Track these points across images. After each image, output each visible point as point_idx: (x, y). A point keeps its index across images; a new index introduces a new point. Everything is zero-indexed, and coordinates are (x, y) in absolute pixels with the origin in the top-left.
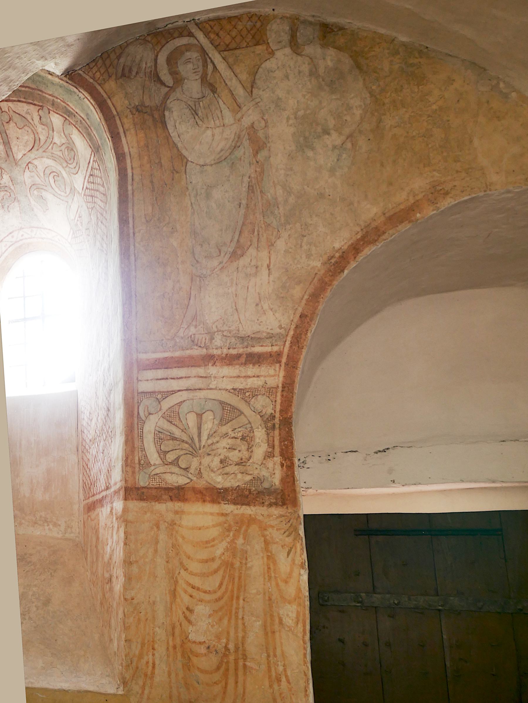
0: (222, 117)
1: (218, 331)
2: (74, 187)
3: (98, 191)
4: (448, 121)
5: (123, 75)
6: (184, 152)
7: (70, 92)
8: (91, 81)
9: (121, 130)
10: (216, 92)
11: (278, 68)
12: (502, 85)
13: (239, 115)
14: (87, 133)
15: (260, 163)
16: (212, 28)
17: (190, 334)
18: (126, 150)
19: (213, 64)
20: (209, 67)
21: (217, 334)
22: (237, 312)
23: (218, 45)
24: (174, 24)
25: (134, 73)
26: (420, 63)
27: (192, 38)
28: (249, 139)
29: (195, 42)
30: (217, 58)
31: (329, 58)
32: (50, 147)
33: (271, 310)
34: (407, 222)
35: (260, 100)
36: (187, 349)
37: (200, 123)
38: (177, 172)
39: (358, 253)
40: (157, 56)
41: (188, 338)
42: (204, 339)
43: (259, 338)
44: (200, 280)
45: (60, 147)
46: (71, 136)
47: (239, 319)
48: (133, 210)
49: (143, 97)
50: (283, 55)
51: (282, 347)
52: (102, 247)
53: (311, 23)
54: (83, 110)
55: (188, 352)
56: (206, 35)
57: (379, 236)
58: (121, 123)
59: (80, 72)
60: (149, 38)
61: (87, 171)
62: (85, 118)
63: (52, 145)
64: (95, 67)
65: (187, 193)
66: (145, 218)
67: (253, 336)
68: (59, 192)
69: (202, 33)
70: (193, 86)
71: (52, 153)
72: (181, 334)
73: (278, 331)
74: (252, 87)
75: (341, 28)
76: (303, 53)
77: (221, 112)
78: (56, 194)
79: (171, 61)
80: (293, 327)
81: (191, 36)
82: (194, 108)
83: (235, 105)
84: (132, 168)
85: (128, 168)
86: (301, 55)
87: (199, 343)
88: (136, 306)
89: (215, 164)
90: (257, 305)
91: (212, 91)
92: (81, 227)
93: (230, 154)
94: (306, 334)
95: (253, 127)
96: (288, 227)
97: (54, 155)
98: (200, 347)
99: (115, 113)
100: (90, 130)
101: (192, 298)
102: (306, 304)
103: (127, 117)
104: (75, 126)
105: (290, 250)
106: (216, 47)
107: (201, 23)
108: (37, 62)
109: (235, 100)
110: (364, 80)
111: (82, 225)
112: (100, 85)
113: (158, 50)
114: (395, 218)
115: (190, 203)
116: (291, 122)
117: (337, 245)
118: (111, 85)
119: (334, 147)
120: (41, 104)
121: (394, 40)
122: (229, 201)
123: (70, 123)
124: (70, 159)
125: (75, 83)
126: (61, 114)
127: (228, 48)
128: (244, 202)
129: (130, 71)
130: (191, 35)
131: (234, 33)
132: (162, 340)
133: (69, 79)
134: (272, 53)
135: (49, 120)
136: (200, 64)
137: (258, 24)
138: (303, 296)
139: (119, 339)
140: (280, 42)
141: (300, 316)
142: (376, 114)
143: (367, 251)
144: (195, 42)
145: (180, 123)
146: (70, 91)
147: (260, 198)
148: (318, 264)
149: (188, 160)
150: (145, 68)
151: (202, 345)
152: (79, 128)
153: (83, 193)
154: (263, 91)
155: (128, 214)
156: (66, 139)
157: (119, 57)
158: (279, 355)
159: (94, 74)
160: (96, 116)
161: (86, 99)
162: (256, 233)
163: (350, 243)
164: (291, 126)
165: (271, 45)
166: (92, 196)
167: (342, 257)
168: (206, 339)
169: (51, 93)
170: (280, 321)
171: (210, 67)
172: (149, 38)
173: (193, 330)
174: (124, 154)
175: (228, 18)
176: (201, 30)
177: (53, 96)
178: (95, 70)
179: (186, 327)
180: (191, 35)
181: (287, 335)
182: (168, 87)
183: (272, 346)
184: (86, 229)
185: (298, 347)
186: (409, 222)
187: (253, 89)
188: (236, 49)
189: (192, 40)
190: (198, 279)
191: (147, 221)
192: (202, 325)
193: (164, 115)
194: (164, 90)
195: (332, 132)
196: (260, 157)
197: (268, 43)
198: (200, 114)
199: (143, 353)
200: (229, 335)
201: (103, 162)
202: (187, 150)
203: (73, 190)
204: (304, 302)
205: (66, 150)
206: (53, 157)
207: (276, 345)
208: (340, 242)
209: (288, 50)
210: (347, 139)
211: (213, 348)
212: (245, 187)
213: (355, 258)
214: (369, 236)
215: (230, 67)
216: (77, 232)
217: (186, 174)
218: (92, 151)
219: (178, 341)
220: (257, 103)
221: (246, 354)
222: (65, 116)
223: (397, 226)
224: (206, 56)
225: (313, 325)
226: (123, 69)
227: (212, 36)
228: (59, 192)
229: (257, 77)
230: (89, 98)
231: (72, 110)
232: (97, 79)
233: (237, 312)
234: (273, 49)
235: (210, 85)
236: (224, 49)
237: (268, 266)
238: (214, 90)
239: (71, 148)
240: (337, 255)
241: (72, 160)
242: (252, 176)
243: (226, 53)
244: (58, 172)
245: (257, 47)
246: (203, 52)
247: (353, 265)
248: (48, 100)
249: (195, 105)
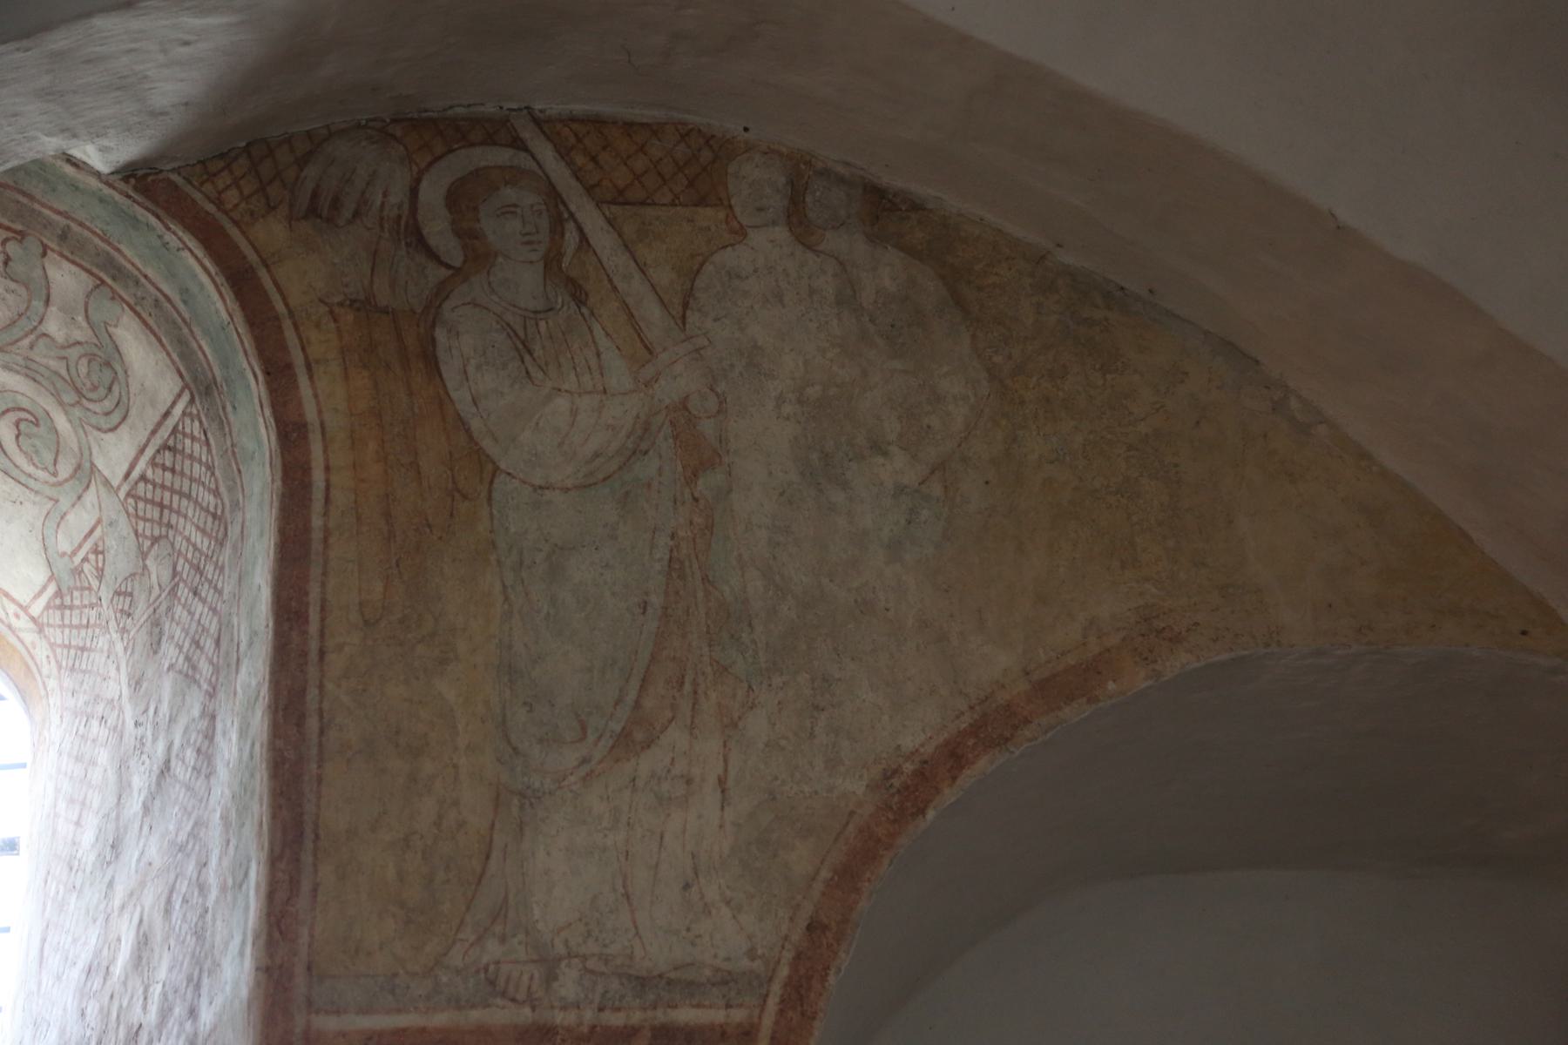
0: (601, 367)
1: (569, 956)
2: (92, 464)
3: (189, 497)
4: (1176, 465)
5: (313, 212)
6: (486, 444)
7: (135, 222)
8: (211, 208)
9: (298, 359)
10: (585, 304)
11: (756, 271)
12: (1294, 403)
13: (649, 371)
14: (172, 331)
15: (702, 502)
16: (579, 140)
17: (485, 960)
18: (311, 414)
19: (580, 230)
20: (567, 235)
21: (568, 966)
22: (630, 905)
23: (593, 187)
24: (472, 109)
25: (347, 213)
26: (1106, 319)
27: (523, 155)
28: (676, 438)
29: (531, 165)
30: (590, 217)
31: (884, 272)
32: (26, 342)
33: (728, 903)
34: (1085, 699)
35: (706, 343)
36: (473, 1006)
37: (537, 374)
38: (465, 497)
39: (962, 768)
40: (418, 181)
41: (478, 972)
42: (525, 978)
43: (691, 984)
44: (522, 807)
45: (63, 348)
46: (111, 329)
47: (634, 922)
48: (323, 584)
49: (372, 282)
50: (769, 244)
51: (757, 1012)
52: (194, 668)
53: (841, 180)
54: (171, 275)
55: (475, 1016)
56: (564, 153)
57: (1015, 727)
58: (300, 338)
59: (174, 177)
60: (398, 131)
61: (154, 432)
62: (176, 298)
63: (32, 337)
64: (225, 173)
65: (493, 558)
66: (362, 614)
67: (673, 975)
68: (30, 469)
69: (550, 146)
70: (522, 280)
71: (27, 359)
72: (456, 958)
73: (745, 963)
74: (686, 306)
75: (917, 206)
76: (821, 248)
77: (598, 355)
78: (15, 473)
79: (459, 199)
80: (788, 955)
81: (518, 148)
82: (521, 334)
83: (639, 344)
84: (327, 469)
85: (313, 464)
86: (817, 253)
87: (511, 989)
88: (315, 865)
89: (576, 487)
90: (687, 886)
91: (574, 296)
92: (95, 583)
93: (620, 468)
94: (824, 978)
95: (686, 408)
96: (777, 680)
97: (34, 366)
98: (513, 1000)
99: (280, 307)
100: (185, 330)
101: (495, 854)
102: (824, 894)
103: (318, 325)
104: (132, 309)
105: (783, 742)
106: (590, 190)
107: (549, 120)
108: (47, 139)
109: (639, 333)
110: (974, 336)
111: (100, 577)
112: (236, 223)
113: (423, 165)
114: (1053, 689)
115: (498, 587)
116: (787, 409)
117: (908, 742)
118: (273, 231)
119: (900, 490)
120: (19, 227)
121: (1043, 257)
122: (613, 594)
123: (115, 297)
124: (95, 388)
125: (156, 203)
126: (88, 266)
127: (620, 198)
128: (656, 600)
129: (336, 204)
130: (518, 144)
131: (640, 164)
132: (395, 975)
133: (135, 189)
134: (741, 233)
135: (40, 272)
136: (544, 223)
137: (706, 155)
138: (817, 872)
139: (248, 963)
140: (760, 209)
141: (809, 928)
142: (1004, 422)
143: (983, 765)
144: (531, 165)
145: (478, 367)
146: (135, 218)
147: (700, 594)
148: (854, 786)
149: (496, 469)
150: (383, 204)
151: (521, 996)
152: (144, 315)
153: (125, 488)
154: (716, 320)
155: (307, 594)
156: (90, 332)
157: (302, 162)
158: (747, 1034)
159: (220, 193)
160: (215, 302)
161: (186, 254)
162: (687, 687)
163: (941, 739)
164: (788, 419)
165: (737, 210)
166: (161, 506)
167: (920, 774)
168: (532, 978)
169: (62, 208)
170: (750, 937)
171: (571, 237)
172: (398, 131)
173: (493, 949)
174: (305, 425)
175: (625, 123)
176: (548, 138)
177: (68, 217)
178: (224, 180)
179: (472, 938)
180: (518, 144)
181: (770, 980)
182: (448, 267)
183: (728, 1006)
184: (118, 593)
185: (803, 1014)
186: (1089, 701)
187: (689, 313)
188: (643, 203)
189: (523, 160)
190: (516, 801)
191: (366, 622)
192: (521, 937)
193: (433, 340)
194: (437, 274)
195: (893, 449)
196: (703, 485)
197: (730, 207)
198: (538, 352)
199: (327, 1012)
200: (603, 969)
201: (222, 428)
202: (496, 440)
203: (85, 473)
204: (818, 887)
205: (84, 361)
206: (30, 372)
207: (741, 1006)
208: (918, 732)
209: (781, 233)
210: (932, 472)
211: (552, 1007)
212: (660, 560)
213: (954, 778)
214: (991, 726)
215: (626, 246)
216: (76, 594)
217: (490, 505)
218: (186, 386)
219: (445, 979)
220: (697, 350)
221: (653, 1029)
222: (102, 275)
223: (1059, 708)
224: (562, 207)
225: (842, 955)
226: (315, 195)
227: (580, 160)
228: (30, 469)
229: (699, 283)
230: (200, 253)
231: (129, 266)
232: (229, 206)
233: (630, 905)
234: (744, 223)
235: (572, 285)
236: (613, 199)
237: (722, 781)
238: (579, 295)
239: (108, 359)
240: (908, 767)
241: (102, 391)
242: (681, 533)
243: (614, 208)
244: (40, 414)
245: (700, 210)
246: (554, 196)
247: (949, 795)
248: (48, 224)
249: (525, 328)
